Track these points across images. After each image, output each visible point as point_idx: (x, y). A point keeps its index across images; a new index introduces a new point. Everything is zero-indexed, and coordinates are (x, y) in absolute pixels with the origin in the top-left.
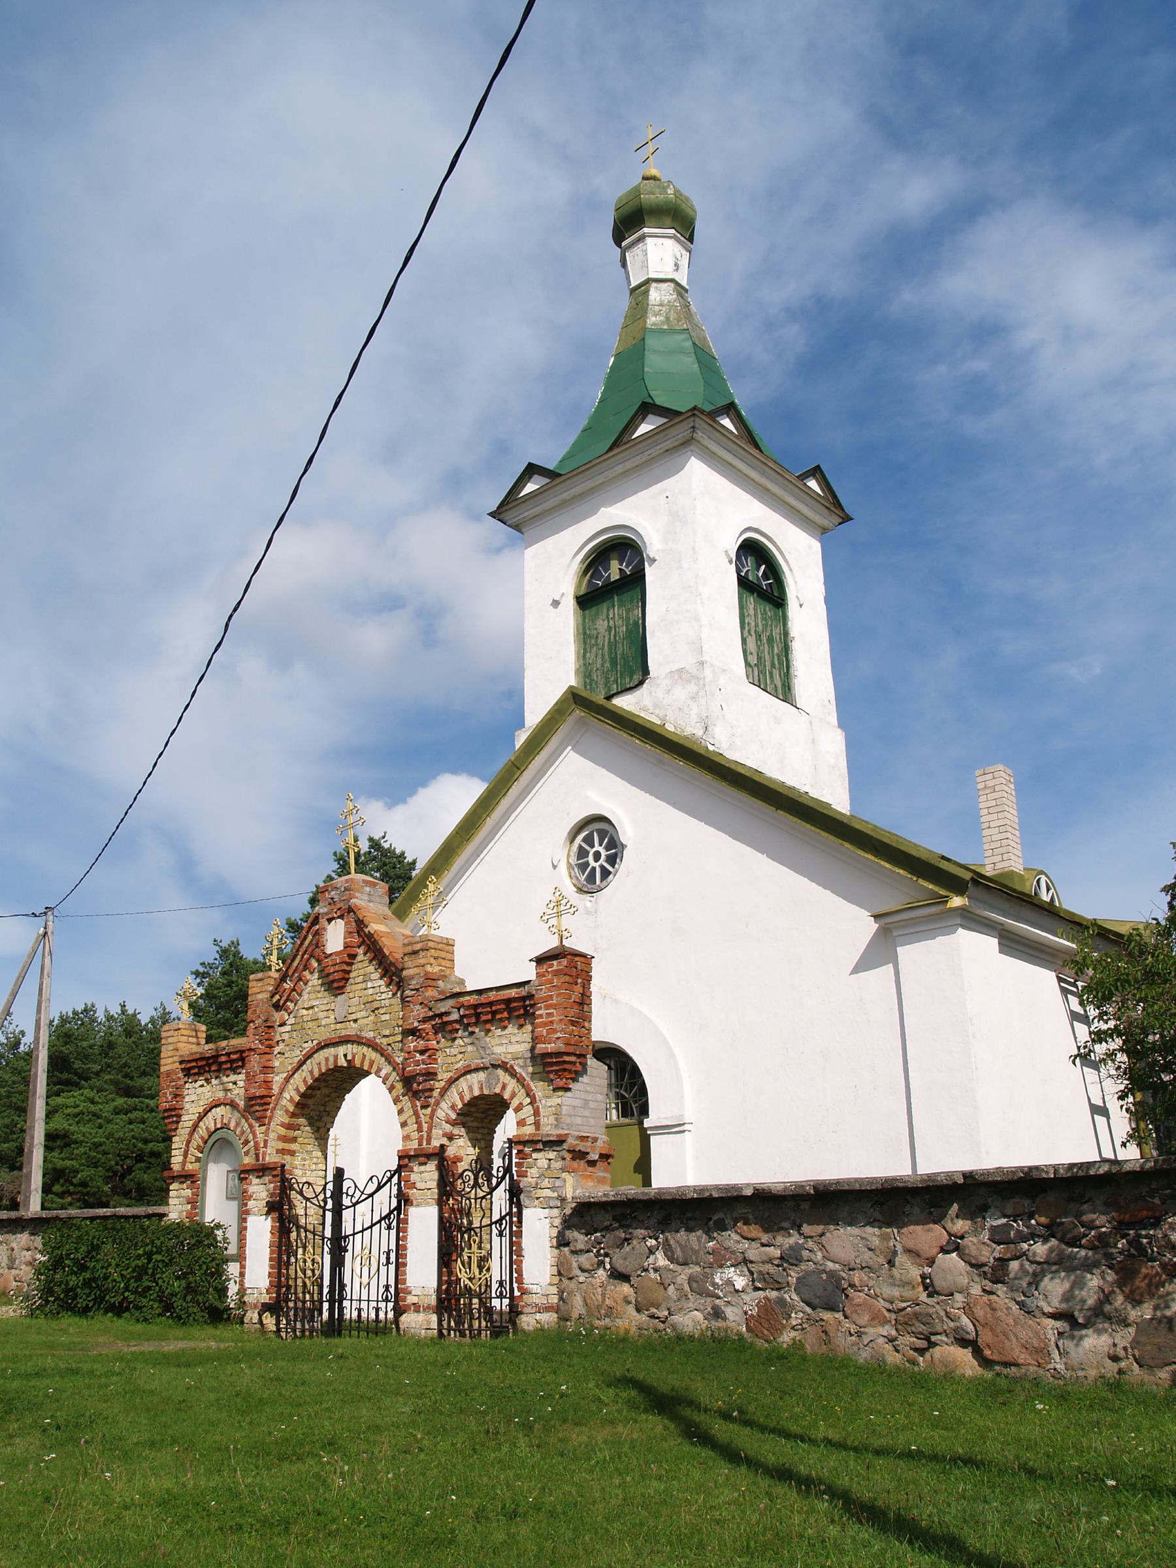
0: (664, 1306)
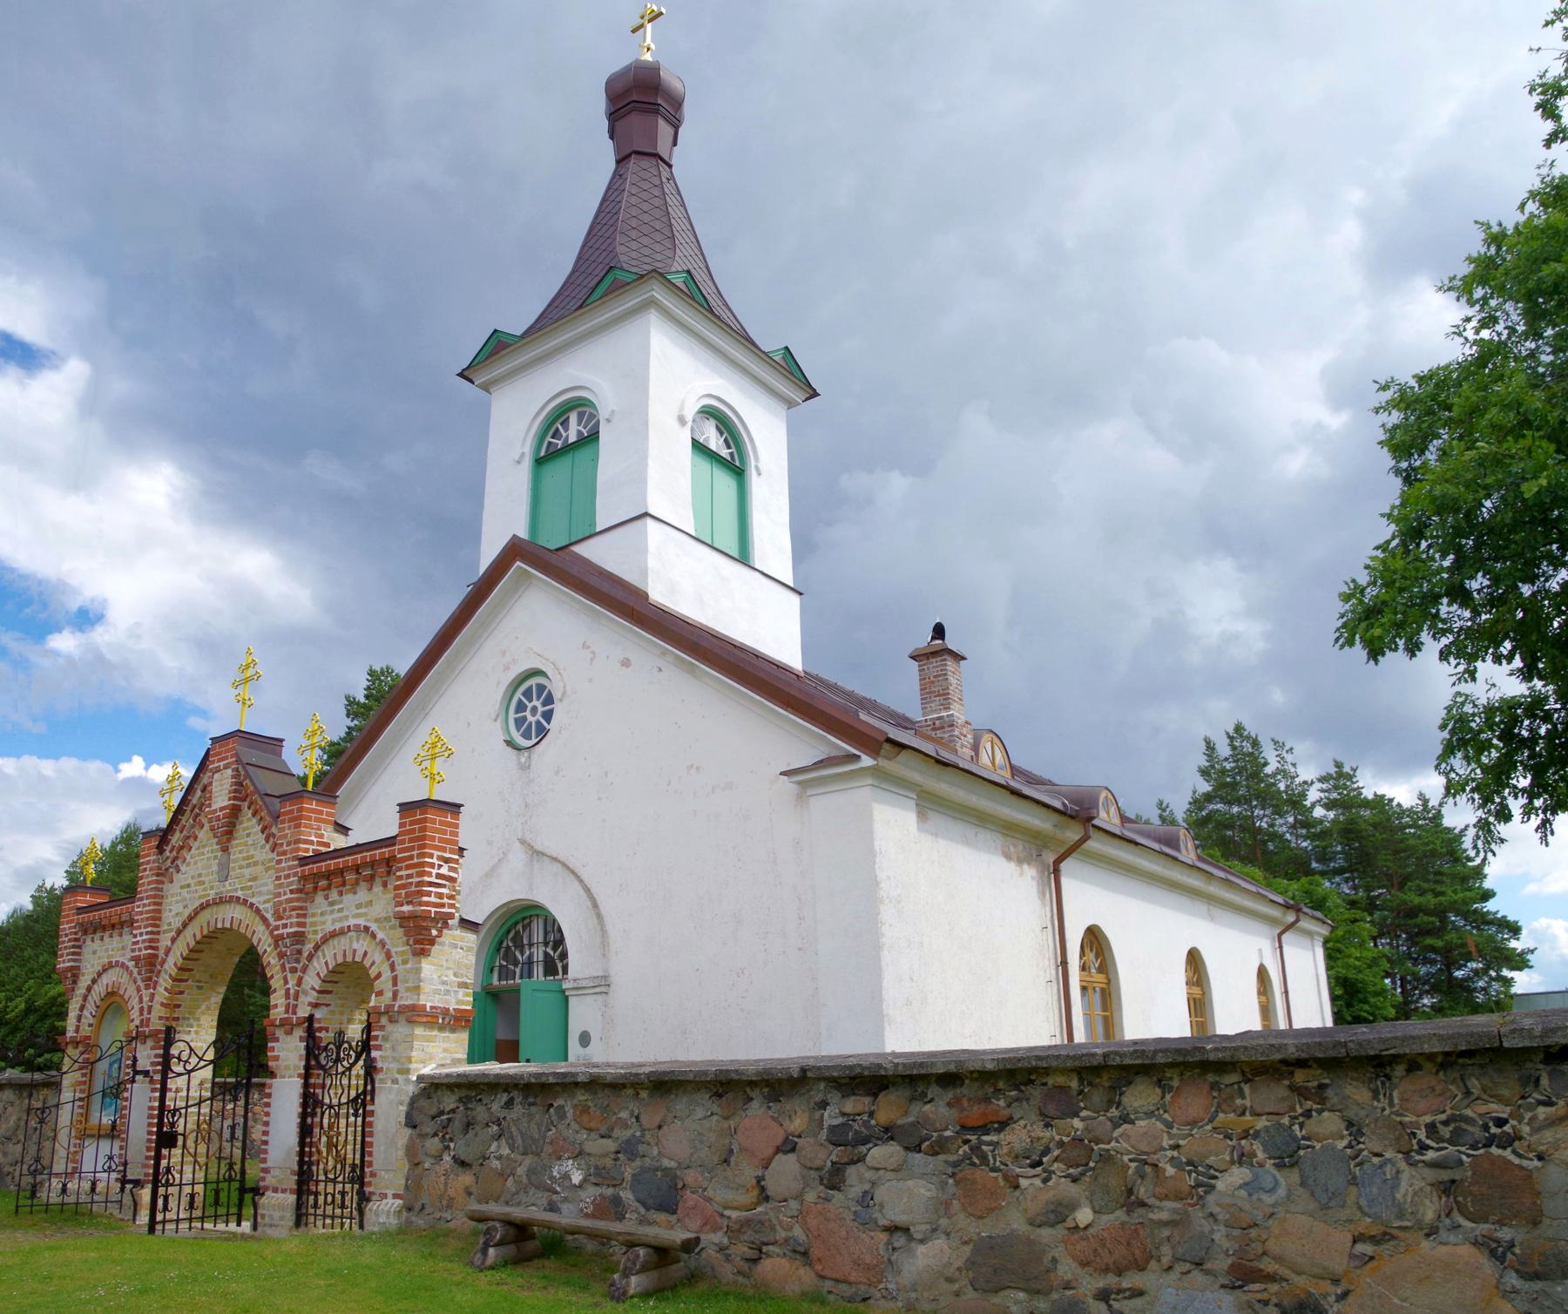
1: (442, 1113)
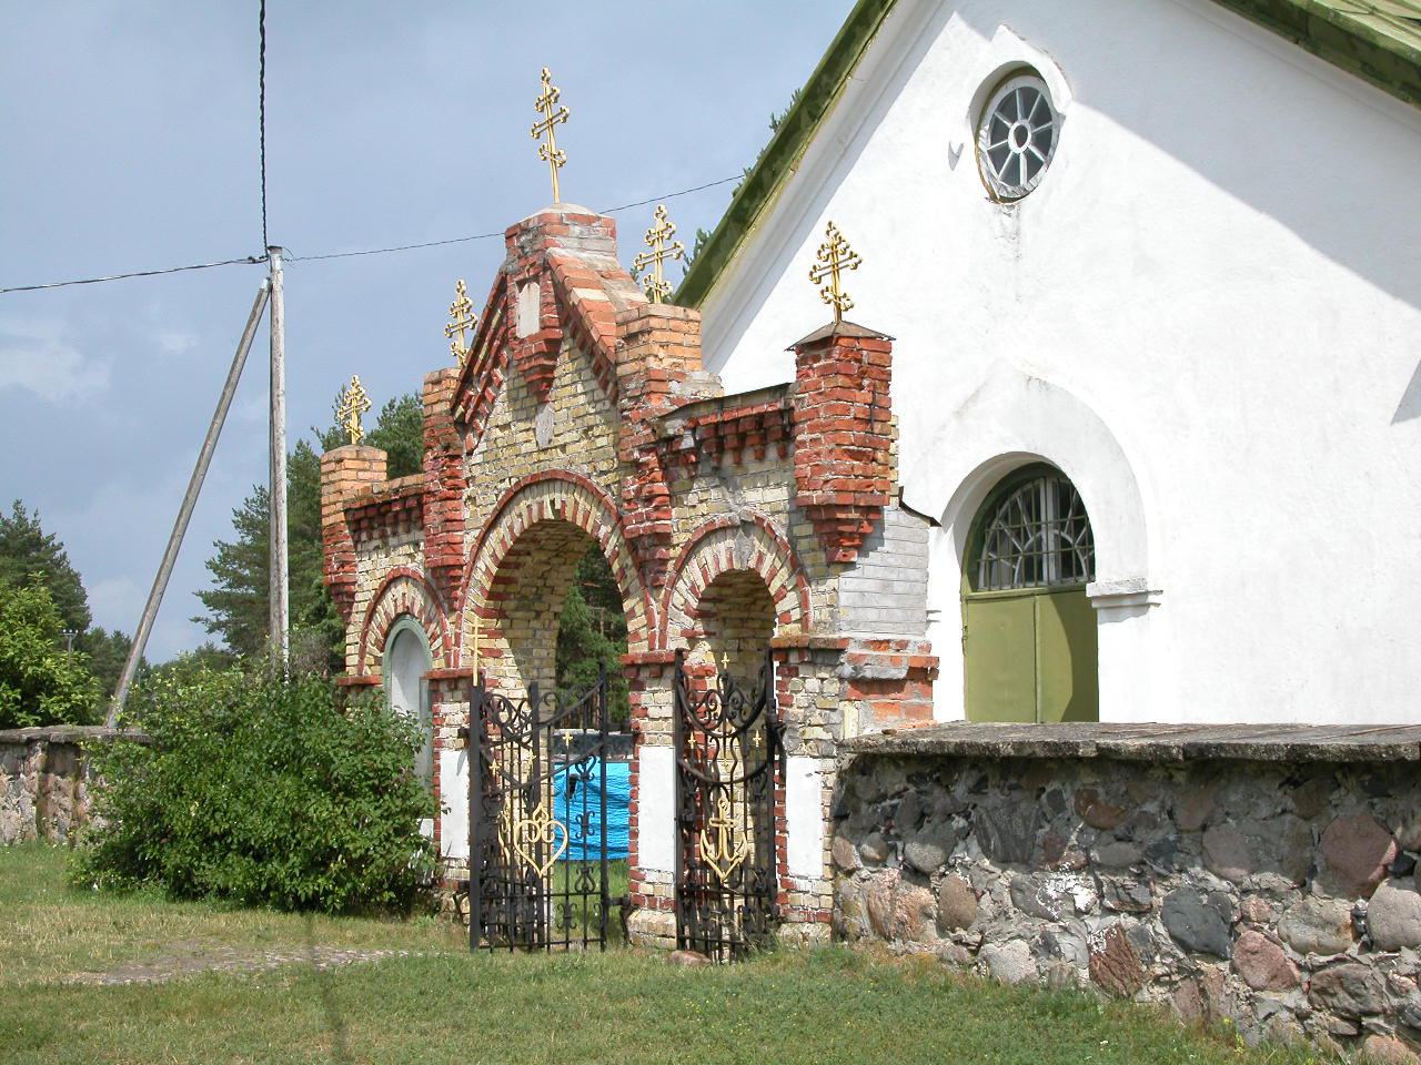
0: (975, 926)
1: (884, 797)
